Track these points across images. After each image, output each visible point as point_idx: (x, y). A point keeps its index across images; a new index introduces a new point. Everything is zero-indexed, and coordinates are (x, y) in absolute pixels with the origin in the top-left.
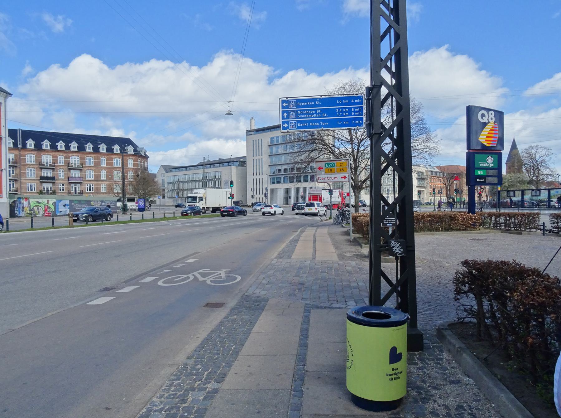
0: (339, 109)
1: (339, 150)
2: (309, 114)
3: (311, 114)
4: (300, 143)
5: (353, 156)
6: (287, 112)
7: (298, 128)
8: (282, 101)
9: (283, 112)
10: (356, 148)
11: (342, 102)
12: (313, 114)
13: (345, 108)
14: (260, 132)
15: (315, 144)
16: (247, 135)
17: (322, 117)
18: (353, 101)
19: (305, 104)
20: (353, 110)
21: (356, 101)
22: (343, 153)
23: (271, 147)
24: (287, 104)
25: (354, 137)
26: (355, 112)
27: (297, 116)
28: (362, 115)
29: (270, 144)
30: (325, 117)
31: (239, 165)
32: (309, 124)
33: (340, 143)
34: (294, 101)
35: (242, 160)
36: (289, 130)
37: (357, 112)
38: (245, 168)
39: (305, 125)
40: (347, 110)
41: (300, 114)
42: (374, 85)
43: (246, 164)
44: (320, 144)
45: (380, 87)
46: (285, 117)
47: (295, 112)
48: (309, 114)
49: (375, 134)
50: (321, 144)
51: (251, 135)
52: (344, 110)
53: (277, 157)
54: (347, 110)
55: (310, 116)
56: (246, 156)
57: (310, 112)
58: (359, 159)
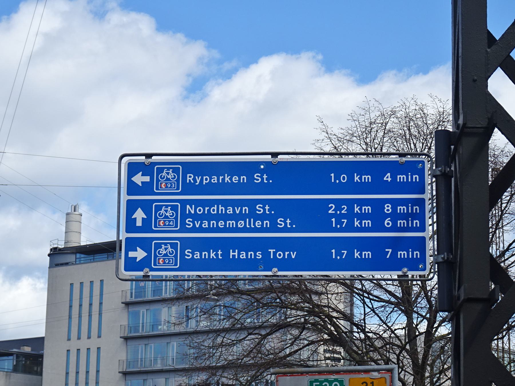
0: (338, 203)
1: (364, 331)
2: (226, 217)
3: (236, 217)
4: (228, 300)
5: (413, 354)
6: (146, 206)
7: (188, 189)
8: (131, 165)
9: (132, 207)
10: (423, 327)
11: (351, 178)
12: (242, 217)
13: (362, 203)
14: (97, 256)
15: (282, 307)
16: (53, 265)
17: (274, 228)
18: (388, 178)
19: (215, 180)
20: (388, 208)
21: (401, 178)
22: (378, 344)
23: (132, 309)
24: (147, 179)
25: (416, 289)
26: (395, 216)
27: (183, 223)
28: (422, 228)
29: (128, 299)
30: (285, 230)
31: (15, 369)
32: (226, 254)
33: (368, 310)
34: (174, 166)
35: (27, 349)
36: (151, 273)
37: (405, 216)
38: (39, 377)
39: (212, 255)
40: (367, 209)
41: (195, 217)
42: (464, 124)
43: (41, 364)
44: (297, 309)
45: (489, 135)
46: (139, 223)
47: (174, 208)
48: (226, 217)
49: (469, 300)
50: (302, 309)
51: (67, 264)
52: (357, 209)
53: (153, 345)
54: (367, 209)
55: (231, 223)
56: (43, 338)
57: (230, 211)
58: (432, 366)
